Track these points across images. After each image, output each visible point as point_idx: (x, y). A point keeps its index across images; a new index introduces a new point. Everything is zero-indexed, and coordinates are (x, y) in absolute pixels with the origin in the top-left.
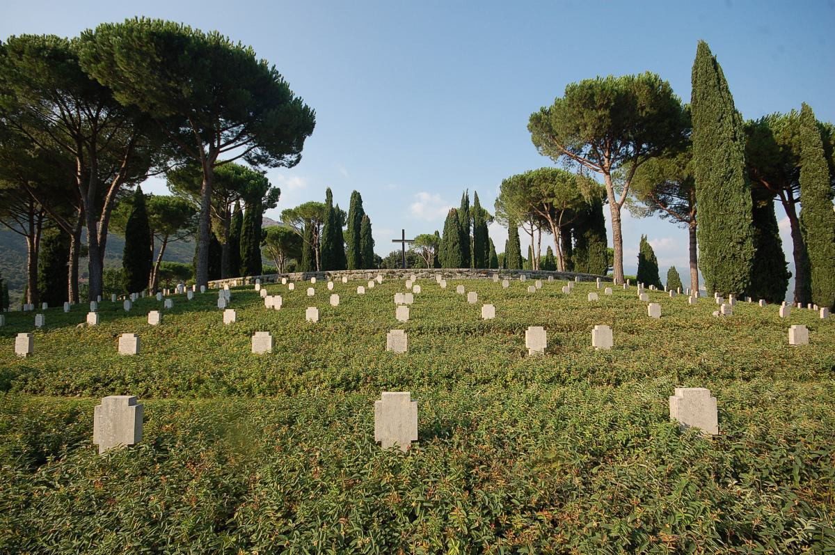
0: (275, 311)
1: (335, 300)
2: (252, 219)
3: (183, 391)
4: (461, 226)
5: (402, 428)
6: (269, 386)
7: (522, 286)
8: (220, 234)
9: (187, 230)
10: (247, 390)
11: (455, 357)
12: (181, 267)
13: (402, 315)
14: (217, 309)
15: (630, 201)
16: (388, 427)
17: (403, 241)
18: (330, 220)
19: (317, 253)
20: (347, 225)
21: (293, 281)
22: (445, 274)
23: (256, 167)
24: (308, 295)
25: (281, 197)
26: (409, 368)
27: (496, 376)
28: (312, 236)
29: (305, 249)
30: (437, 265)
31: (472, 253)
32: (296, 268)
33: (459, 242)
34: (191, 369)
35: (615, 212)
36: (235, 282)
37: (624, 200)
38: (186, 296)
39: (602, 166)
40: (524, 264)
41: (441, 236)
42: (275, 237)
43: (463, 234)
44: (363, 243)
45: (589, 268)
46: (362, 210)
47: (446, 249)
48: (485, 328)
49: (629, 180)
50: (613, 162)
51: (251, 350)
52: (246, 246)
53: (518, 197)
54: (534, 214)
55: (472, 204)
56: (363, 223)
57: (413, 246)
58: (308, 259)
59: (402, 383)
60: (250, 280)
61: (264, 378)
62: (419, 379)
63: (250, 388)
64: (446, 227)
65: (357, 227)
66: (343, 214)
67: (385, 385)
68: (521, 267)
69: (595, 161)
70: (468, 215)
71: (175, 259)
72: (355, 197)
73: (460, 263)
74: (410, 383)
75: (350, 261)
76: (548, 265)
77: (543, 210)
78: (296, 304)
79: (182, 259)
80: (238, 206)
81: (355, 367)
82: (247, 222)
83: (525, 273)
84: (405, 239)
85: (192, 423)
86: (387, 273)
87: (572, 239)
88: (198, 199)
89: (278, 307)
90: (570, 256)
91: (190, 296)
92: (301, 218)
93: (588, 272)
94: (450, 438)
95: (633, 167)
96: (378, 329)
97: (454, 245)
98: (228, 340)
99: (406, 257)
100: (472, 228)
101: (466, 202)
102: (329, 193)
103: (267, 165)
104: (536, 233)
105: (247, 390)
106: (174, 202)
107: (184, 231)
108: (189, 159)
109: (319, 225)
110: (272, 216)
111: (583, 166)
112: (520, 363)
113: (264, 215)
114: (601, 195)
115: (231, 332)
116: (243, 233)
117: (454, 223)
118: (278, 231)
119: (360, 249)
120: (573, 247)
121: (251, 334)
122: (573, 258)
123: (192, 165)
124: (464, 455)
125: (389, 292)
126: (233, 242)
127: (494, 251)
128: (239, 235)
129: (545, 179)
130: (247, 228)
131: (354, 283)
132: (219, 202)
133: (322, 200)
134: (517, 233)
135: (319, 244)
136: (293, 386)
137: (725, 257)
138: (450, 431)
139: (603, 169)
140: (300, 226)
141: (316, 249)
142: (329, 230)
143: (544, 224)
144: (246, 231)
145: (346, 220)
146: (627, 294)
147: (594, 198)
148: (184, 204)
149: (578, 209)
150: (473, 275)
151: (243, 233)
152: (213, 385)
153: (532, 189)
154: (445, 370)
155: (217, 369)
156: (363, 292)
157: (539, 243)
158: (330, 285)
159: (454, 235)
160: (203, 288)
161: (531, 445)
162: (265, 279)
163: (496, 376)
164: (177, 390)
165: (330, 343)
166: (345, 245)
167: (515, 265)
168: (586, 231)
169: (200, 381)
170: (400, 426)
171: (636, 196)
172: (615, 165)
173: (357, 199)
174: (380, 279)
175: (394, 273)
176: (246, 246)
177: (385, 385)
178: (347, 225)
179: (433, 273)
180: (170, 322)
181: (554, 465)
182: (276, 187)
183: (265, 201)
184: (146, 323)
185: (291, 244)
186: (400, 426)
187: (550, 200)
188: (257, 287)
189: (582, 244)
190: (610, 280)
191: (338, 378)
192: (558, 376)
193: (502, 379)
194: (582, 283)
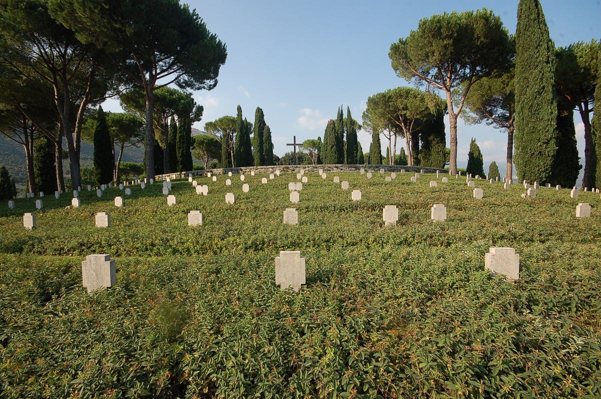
1: (246, 188)
6: (201, 248)
10: (186, 251)
12: (135, 166)
13: (295, 198)
14: (163, 195)
17: (295, 145)
18: (241, 130)
19: (232, 154)
20: (253, 133)
21: (216, 175)
22: (325, 168)
25: (204, 113)
26: (299, 235)
27: (361, 240)
28: (228, 142)
29: (223, 152)
30: (320, 162)
31: (345, 153)
32: (217, 166)
35: (453, 120)
36: (174, 176)
37: (460, 111)
38: (141, 186)
39: (445, 85)
40: (383, 161)
41: (323, 141)
42: (201, 143)
43: (339, 139)
44: (265, 146)
48: (354, 207)
51: (188, 223)
55: (345, 116)
56: (265, 131)
59: (294, 245)
60: (185, 174)
61: (198, 242)
62: (306, 243)
63: (188, 250)
64: (326, 134)
66: (250, 125)
67: (283, 247)
68: (381, 163)
69: (439, 81)
72: (259, 112)
75: (256, 159)
76: (401, 162)
79: (135, 160)
80: (173, 120)
81: (261, 235)
82: (180, 132)
83: (384, 167)
87: (420, 141)
89: (205, 193)
90: (417, 154)
91: (143, 187)
92: (219, 128)
94: (328, 282)
97: (332, 147)
99: (297, 156)
100: (345, 134)
101: (341, 115)
102: (239, 109)
103: (192, 88)
104: (393, 138)
105: (186, 251)
106: (127, 117)
107: (135, 139)
109: (233, 134)
110: (198, 127)
113: (192, 127)
114: (443, 107)
115: (173, 211)
116: (178, 140)
118: (204, 139)
120: (420, 148)
122: (420, 156)
126: (171, 147)
127: (362, 152)
128: (175, 142)
129: (401, 96)
130: (180, 137)
131: (259, 176)
133: (234, 114)
134: (379, 138)
136: (218, 248)
137: (534, 153)
138: (328, 278)
139: (446, 87)
140: (219, 134)
143: (399, 131)
145: (252, 129)
147: (438, 110)
148: (134, 119)
149: (425, 119)
150: (346, 170)
151: (178, 140)
157: (395, 145)
158: (242, 178)
160: (151, 181)
162: (196, 174)
163: (361, 240)
166: (252, 148)
169: (153, 245)
173: (260, 114)
174: (278, 173)
175: (288, 168)
177: (283, 247)
178: (253, 133)
179: (316, 168)
180: (130, 204)
182: (200, 105)
183: (193, 116)
184: (113, 205)
186: (293, 275)
188: (190, 179)
189: (427, 146)
190: (446, 172)
191: (249, 243)
193: (366, 242)
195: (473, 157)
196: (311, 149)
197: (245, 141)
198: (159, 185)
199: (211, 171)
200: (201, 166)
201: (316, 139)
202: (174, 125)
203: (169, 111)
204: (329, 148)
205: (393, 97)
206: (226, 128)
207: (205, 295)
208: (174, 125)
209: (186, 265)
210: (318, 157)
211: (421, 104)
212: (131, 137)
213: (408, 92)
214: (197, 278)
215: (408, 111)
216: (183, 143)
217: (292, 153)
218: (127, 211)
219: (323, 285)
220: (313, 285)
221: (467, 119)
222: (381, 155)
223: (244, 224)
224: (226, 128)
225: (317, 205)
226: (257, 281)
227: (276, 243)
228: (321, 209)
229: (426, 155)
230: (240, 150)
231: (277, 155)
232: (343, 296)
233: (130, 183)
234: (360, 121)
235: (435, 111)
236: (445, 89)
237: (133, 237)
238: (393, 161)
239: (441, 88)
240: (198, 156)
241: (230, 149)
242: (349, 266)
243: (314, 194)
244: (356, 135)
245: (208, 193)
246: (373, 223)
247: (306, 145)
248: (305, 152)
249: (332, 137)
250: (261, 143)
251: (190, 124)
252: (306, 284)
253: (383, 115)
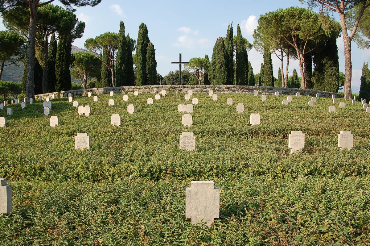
0: (86, 117)
1: (131, 109)
2: (64, 47)
3: (31, 176)
4: (227, 51)
5: (208, 208)
6: (92, 175)
7: (277, 99)
8: (41, 59)
9: (17, 56)
10: (76, 177)
11: (235, 156)
12: (14, 85)
13: (187, 120)
14: (44, 116)
15: (358, 36)
16: (196, 208)
17: (180, 63)
18: (123, 47)
19: (112, 72)
20: (136, 50)
21: (96, 95)
22: (216, 89)
23: (69, 7)
24: (109, 105)
25: (85, 30)
26: (200, 163)
27: (269, 169)
28: (108, 59)
29: (103, 70)
30: (207, 81)
31: (235, 73)
32: (96, 85)
33: (225, 64)
34: (35, 160)
35: (347, 43)
36: (53, 96)
37: (354, 34)
38: (21, 106)
39: (338, 7)
40: (275, 83)
41: (210, 59)
42: (81, 61)
43: (228, 59)
44: (148, 64)
45: (325, 87)
46: (148, 38)
47: (215, 70)
48: (254, 133)
49: (359, 19)
50: (347, 4)
51: (74, 147)
52: (60, 68)
53: (273, 29)
54: (284, 43)
55: (235, 34)
56: (149, 49)
57: (187, 67)
58: (106, 78)
59: (196, 175)
60: (64, 94)
61: (88, 168)
62: (208, 171)
63: (78, 176)
64: (214, 53)
65: (143, 52)
66: (133, 41)
67: (182, 176)
68: (273, 85)
69: (332, 3)
70: (232, 43)
71: (9, 79)
73: (225, 80)
74: (202, 174)
75: (138, 77)
76: (293, 84)
77: (291, 40)
78: (101, 112)
79: (14, 79)
80: (53, 37)
81: (156, 162)
82: (60, 50)
83: (278, 90)
84: (182, 61)
85: (43, 200)
86: (170, 89)
87: (313, 64)
88: (25, 33)
89: (87, 114)
90: (310, 77)
91: (23, 106)
92: (100, 45)
93: (324, 90)
94: (243, 216)
95: (362, 8)
96: (169, 132)
97: (220, 67)
98: (56, 139)
99: (182, 75)
100: (235, 53)
101: (230, 32)
102: (122, 25)
103: (76, 5)
104: (285, 58)
105: (76, 177)
106: (8, 35)
107: (15, 57)
108: (19, 2)
109: (114, 51)
110: (78, 44)
111: (324, 6)
112: (287, 159)
113: (73, 44)
114: (338, 30)
115: (56, 133)
116: (57, 58)
117: (221, 49)
118: (83, 56)
119: (146, 69)
120: (313, 70)
121: (72, 134)
122: (313, 79)
123: (21, 7)
124: (258, 229)
125: (172, 103)
126: (51, 65)
127: (252, 72)
128: (55, 60)
129: (294, 16)
130: (60, 54)
131: (143, 96)
132: (40, 35)
133: (116, 31)
135: (114, 66)
136: (110, 175)
138: (244, 212)
139: (339, 10)
140: (99, 52)
141: (112, 69)
142: (122, 54)
143: (291, 52)
144: (60, 57)
145: (135, 46)
146: (355, 108)
147: (332, 32)
148: (15, 37)
149: (318, 41)
150: (237, 91)
151: (57, 58)
152: (52, 173)
153: (284, 23)
154: (229, 164)
155: (53, 160)
156: (152, 103)
157: (288, 67)
158: (125, 98)
159: (221, 58)
160: (31, 100)
161: (307, 221)
162: (75, 93)
163: (269, 169)
164: (26, 175)
165: (133, 142)
166: (134, 66)
167: (268, 83)
168: (323, 58)
169: (42, 169)
170: (206, 208)
171: (362, 32)
172: (348, 6)
173: (144, 30)
174: (164, 93)
175: (174, 88)
176: (60, 68)
177: (182, 176)
178: (136, 50)
179: (206, 88)
180: (13, 125)
181: (325, 236)
182: (82, 22)
183: (74, 33)
185: (92, 66)
186: (206, 208)
187: (297, 33)
188: (70, 99)
189: (320, 69)
190: (341, 96)
191: (145, 170)
192: (316, 169)
193: (273, 171)
194: (321, 98)
195: (365, 81)
196: (198, 68)
197: (126, 59)
198: (38, 105)
199: (91, 91)
200: (79, 85)
201: (203, 57)
202: (54, 43)
203: (51, 29)
204: (218, 67)
205: (286, 16)
206: (108, 44)
207: (108, 228)
208: (54, 43)
209: (80, 193)
210: (204, 77)
211: (314, 25)
212: (12, 55)
213: (301, 12)
214: (95, 208)
215: (301, 32)
216: (63, 61)
217: (177, 72)
218: (10, 132)
219: (239, 219)
220: (228, 219)
221: (360, 43)
222: (273, 76)
223: (135, 149)
224: (108, 44)
225: (213, 129)
226: (163, 214)
227: (175, 171)
228: (217, 134)
229: (319, 78)
230: (121, 68)
231: (161, 74)
232: (263, 232)
233: (9, 103)
234: (251, 40)
235: (330, 34)
236: (338, 11)
237: (21, 159)
238: (286, 83)
239: (334, 10)
240: (76, 74)
241: (111, 67)
242: (264, 198)
243: (208, 118)
244: (247, 54)
245: (90, 114)
246: (277, 150)
247: (192, 63)
248: (191, 71)
249: (221, 55)
250: (144, 61)
251: (70, 41)
252: (220, 218)
253: (275, 34)
